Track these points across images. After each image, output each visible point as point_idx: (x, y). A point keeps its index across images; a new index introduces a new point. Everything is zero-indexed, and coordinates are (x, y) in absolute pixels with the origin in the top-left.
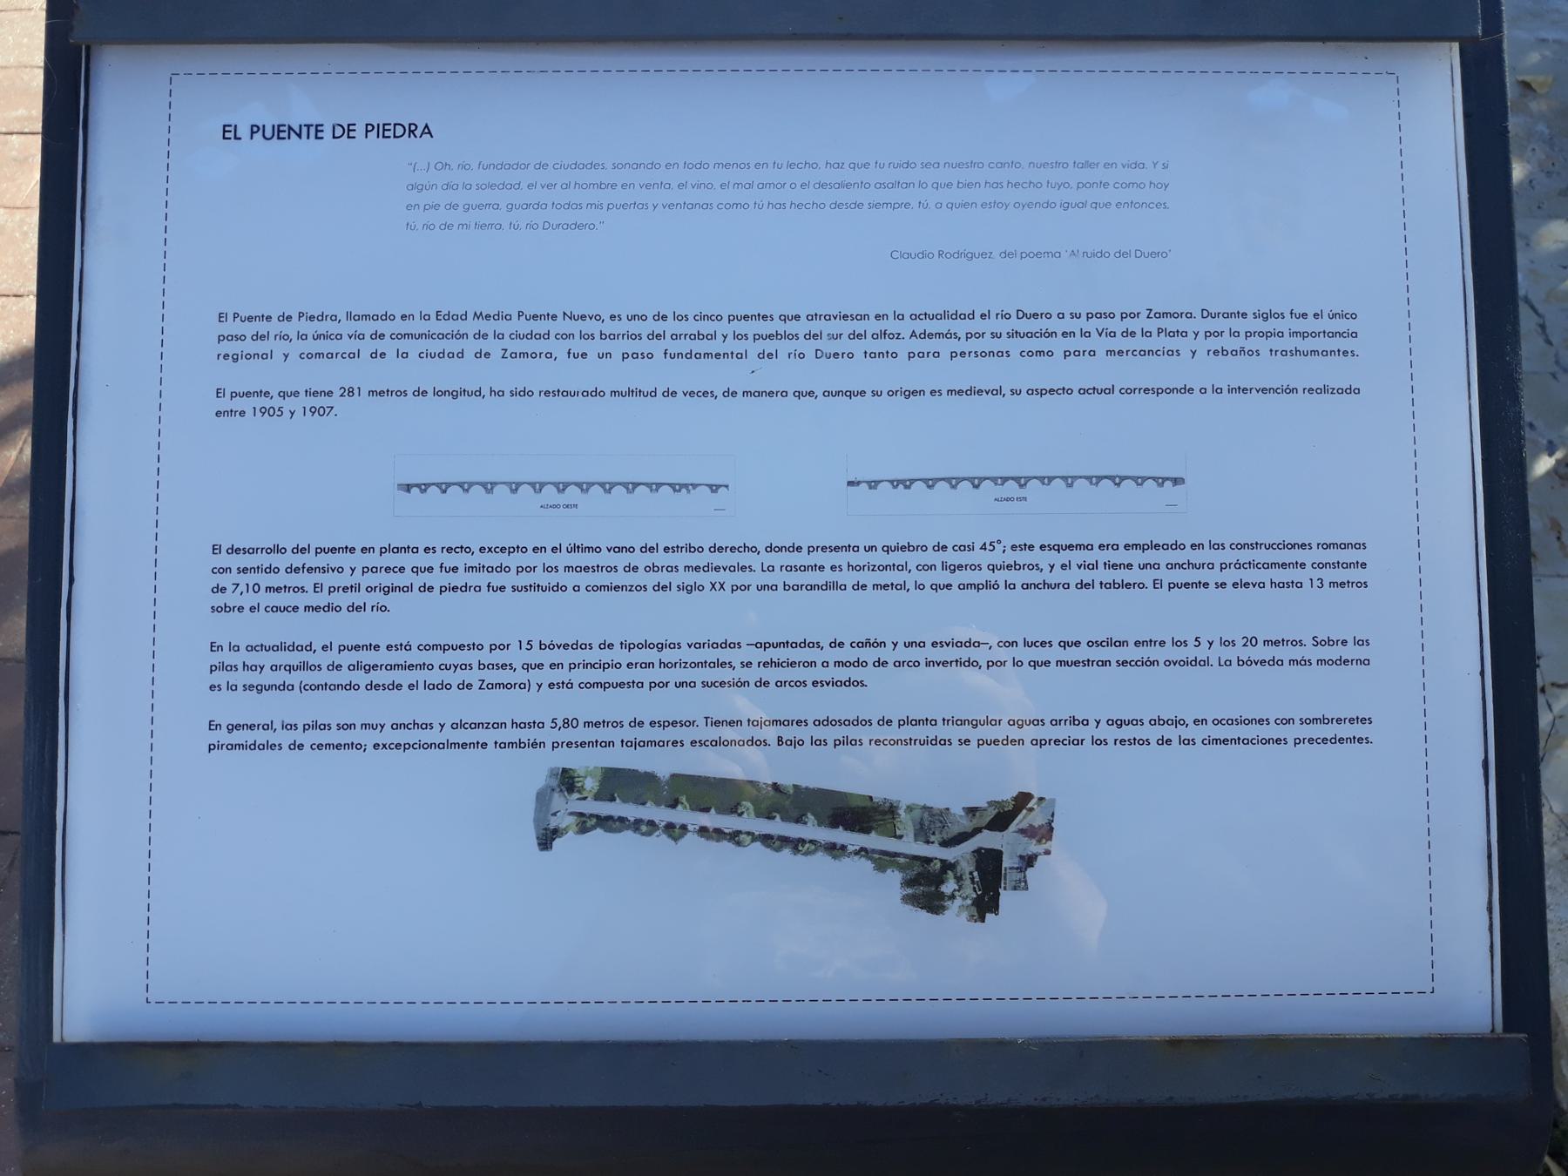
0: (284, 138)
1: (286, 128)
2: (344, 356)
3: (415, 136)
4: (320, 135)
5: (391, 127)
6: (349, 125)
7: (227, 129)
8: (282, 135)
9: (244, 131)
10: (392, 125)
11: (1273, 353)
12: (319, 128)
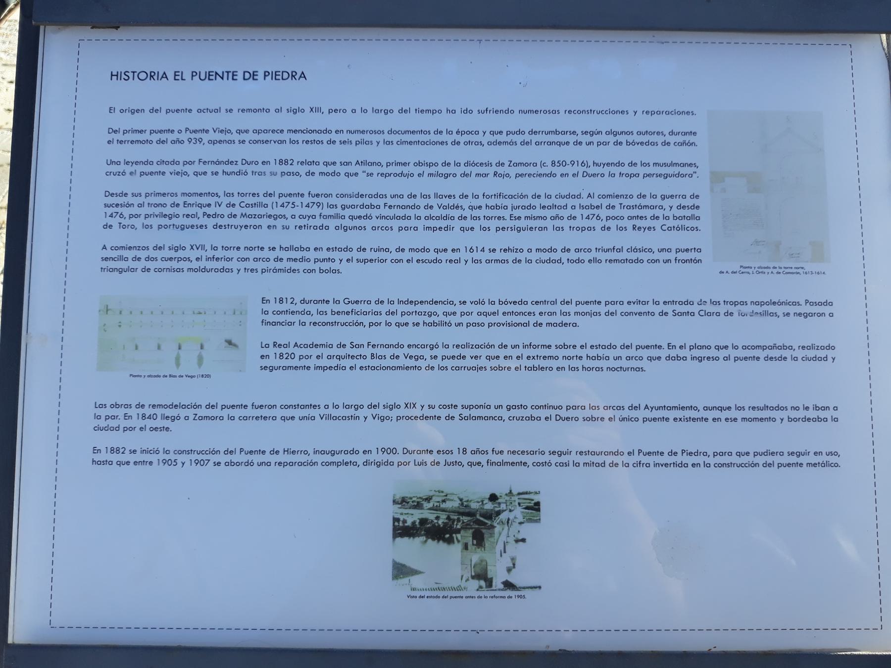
0: (212, 80)
1: (214, 74)
2: (383, 228)
3: (154, 79)
4: (235, 77)
5: (281, 73)
6: (254, 72)
7: (177, 74)
8: (211, 77)
9: (187, 75)
10: (281, 72)
11: (572, 229)
12: (235, 73)
